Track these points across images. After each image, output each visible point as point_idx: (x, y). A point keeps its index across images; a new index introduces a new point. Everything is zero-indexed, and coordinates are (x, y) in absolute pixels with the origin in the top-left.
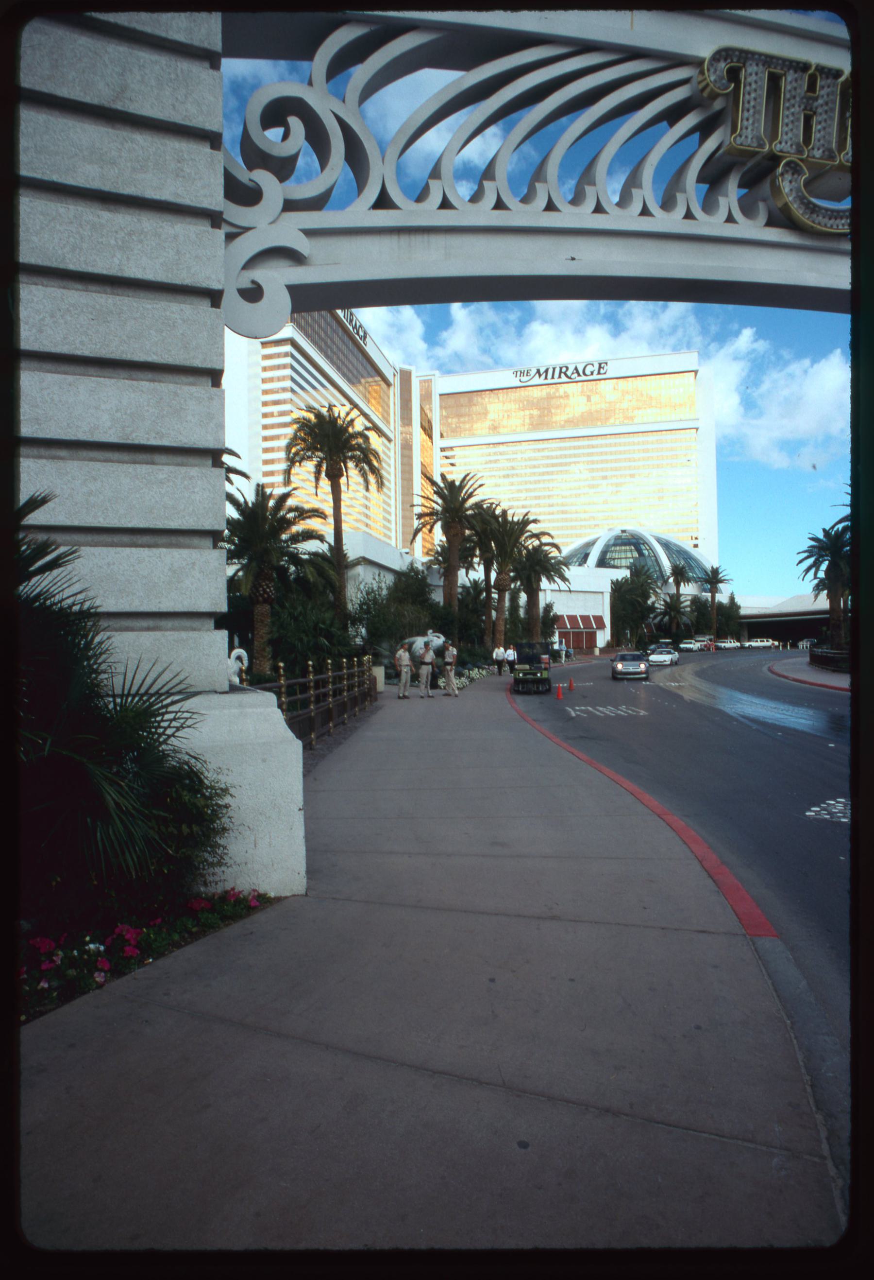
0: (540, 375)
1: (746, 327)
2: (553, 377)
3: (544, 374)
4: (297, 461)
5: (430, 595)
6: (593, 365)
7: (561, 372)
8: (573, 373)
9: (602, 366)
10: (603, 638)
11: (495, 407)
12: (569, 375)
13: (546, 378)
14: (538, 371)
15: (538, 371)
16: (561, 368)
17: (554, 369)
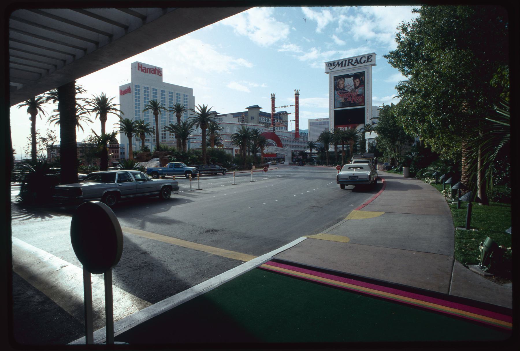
0: (339, 65)
1: (75, 98)
2: (345, 66)
3: (341, 65)
4: (457, 54)
5: (168, 149)
7: (349, 63)
8: (355, 63)
9: (369, 57)
10: (336, 129)
11: (189, 109)
12: (353, 64)
13: (342, 66)
16: (349, 60)
17: (346, 61)
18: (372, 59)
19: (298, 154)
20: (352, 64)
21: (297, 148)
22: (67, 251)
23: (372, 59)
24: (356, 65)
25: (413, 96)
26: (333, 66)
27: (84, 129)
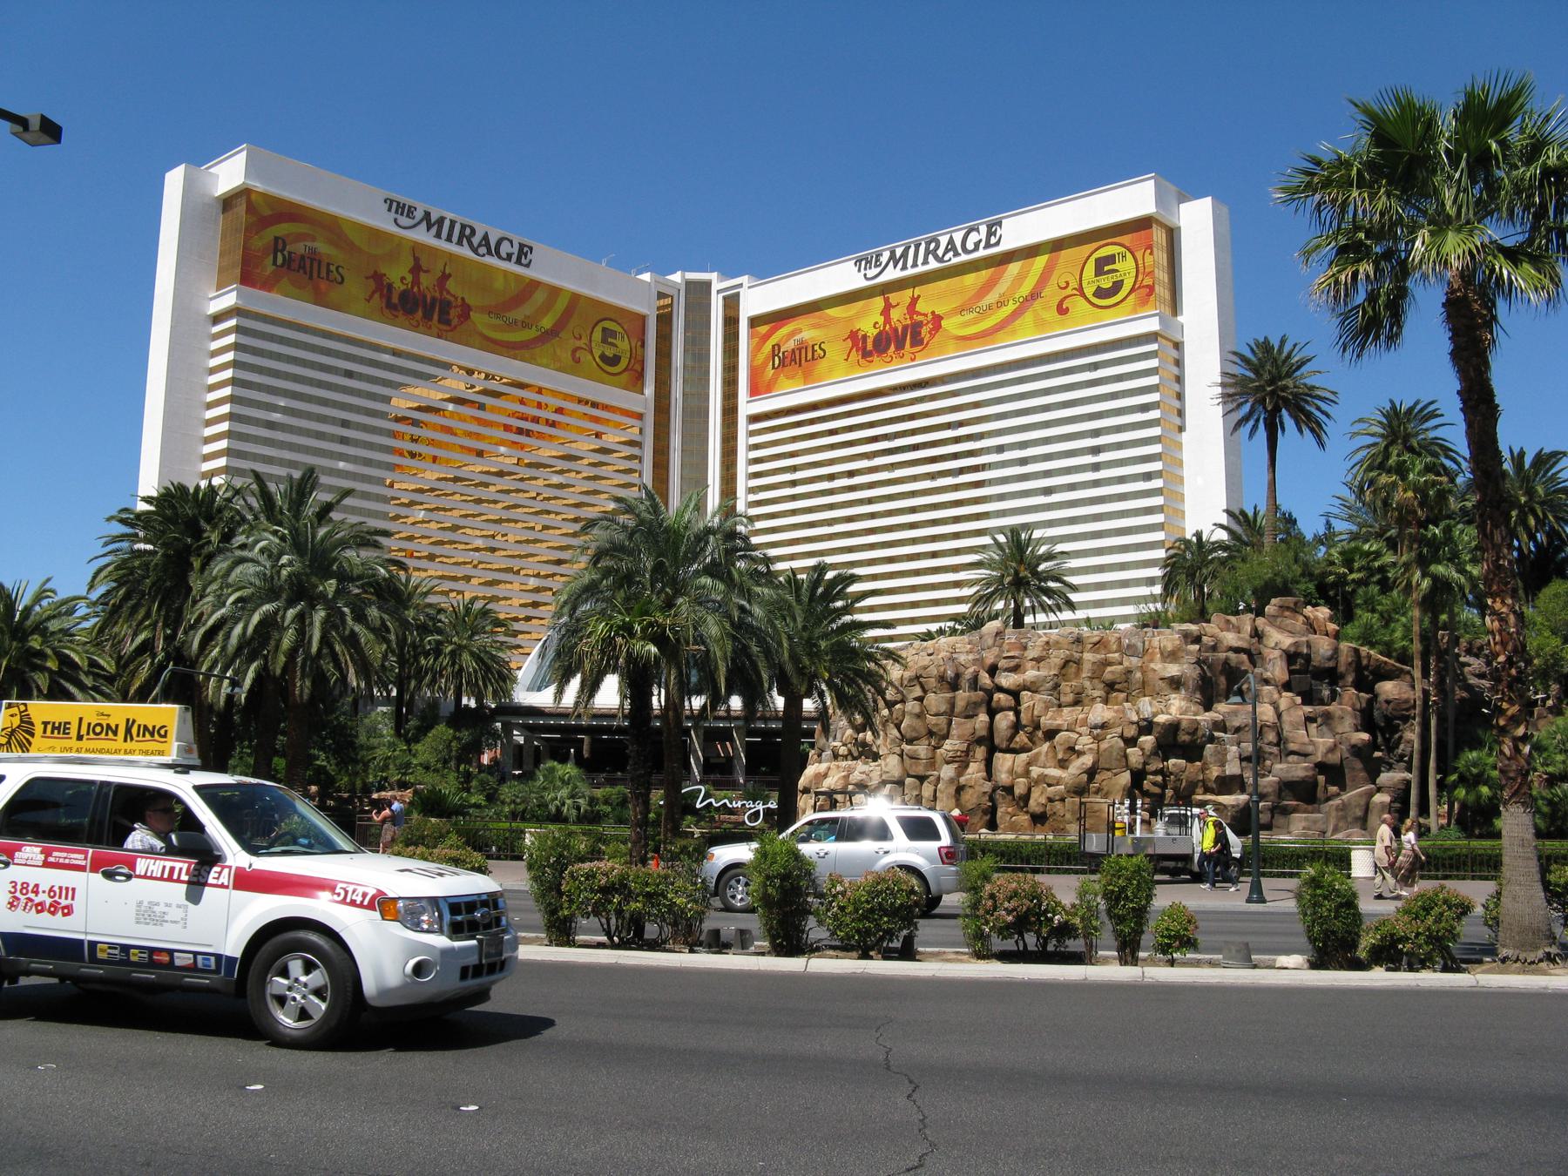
2: (915, 265)
3: (435, 228)
6: (511, 242)
7: (462, 235)
8: (480, 245)
12: (475, 245)
13: (438, 235)
14: (427, 215)
15: (427, 215)
16: (463, 227)
18: (1001, 236)
19: (440, 790)
20: (936, 258)
21: (1060, 610)
22: (1309, 603)
23: (1001, 236)
24: (484, 255)
25: (174, 602)
26: (876, 266)
27: (1431, 400)
